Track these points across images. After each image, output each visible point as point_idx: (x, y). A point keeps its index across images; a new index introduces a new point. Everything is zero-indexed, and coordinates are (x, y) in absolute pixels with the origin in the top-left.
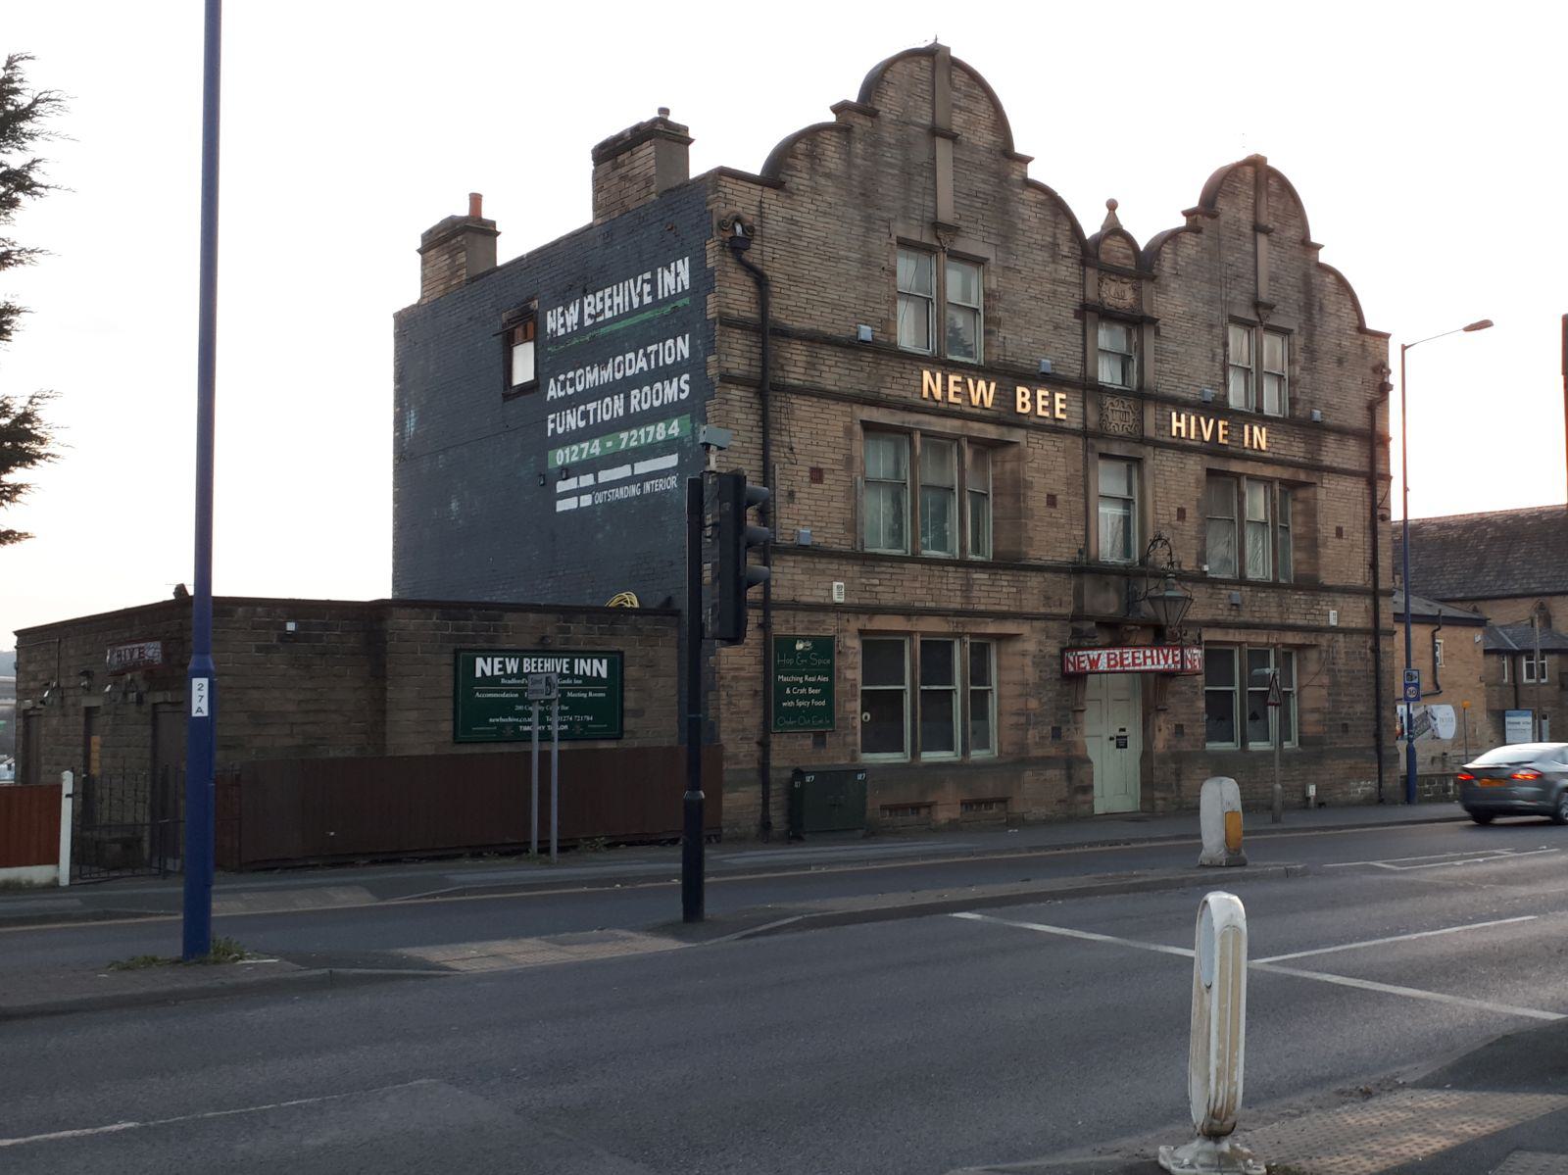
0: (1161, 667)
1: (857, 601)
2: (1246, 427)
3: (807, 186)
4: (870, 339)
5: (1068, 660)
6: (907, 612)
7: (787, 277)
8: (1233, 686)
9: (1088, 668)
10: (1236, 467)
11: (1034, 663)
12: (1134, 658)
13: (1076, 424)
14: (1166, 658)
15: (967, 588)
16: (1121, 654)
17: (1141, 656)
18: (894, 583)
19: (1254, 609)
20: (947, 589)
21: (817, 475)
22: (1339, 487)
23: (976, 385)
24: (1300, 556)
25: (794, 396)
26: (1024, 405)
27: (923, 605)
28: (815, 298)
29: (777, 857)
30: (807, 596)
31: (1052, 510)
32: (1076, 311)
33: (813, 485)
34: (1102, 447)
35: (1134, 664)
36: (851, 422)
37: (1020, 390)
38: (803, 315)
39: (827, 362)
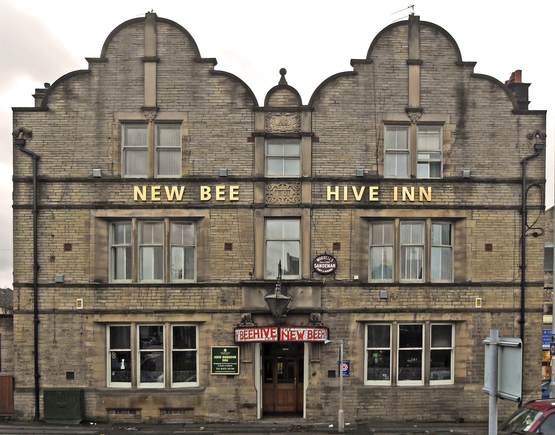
0: (264, 339)
1: (92, 308)
2: (396, 189)
3: (63, 106)
4: (100, 175)
5: (283, 333)
6: (125, 312)
7: (51, 153)
8: (196, 348)
9: (297, 339)
10: (384, 213)
11: (214, 337)
12: (250, 334)
13: (248, 201)
14: (267, 335)
15: (165, 299)
16: (314, 331)
17: (253, 333)
18: (116, 298)
19: (401, 300)
20: (151, 299)
21: (68, 247)
22: (489, 218)
23: (170, 189)
24: (458, 264)
25: (55, 210)
26: (206, 196)
27: (135, 308)
28: (68, 160)
29: (34, 428)
30: (62, 307)
31: (229, 252)
32: (248, 138)
33: (66, 252)
34: (266, 212)
35: (250, 338)
36: (89, 219)
37: (203, 188)
38: (61, 170)
39: (74, 191)
